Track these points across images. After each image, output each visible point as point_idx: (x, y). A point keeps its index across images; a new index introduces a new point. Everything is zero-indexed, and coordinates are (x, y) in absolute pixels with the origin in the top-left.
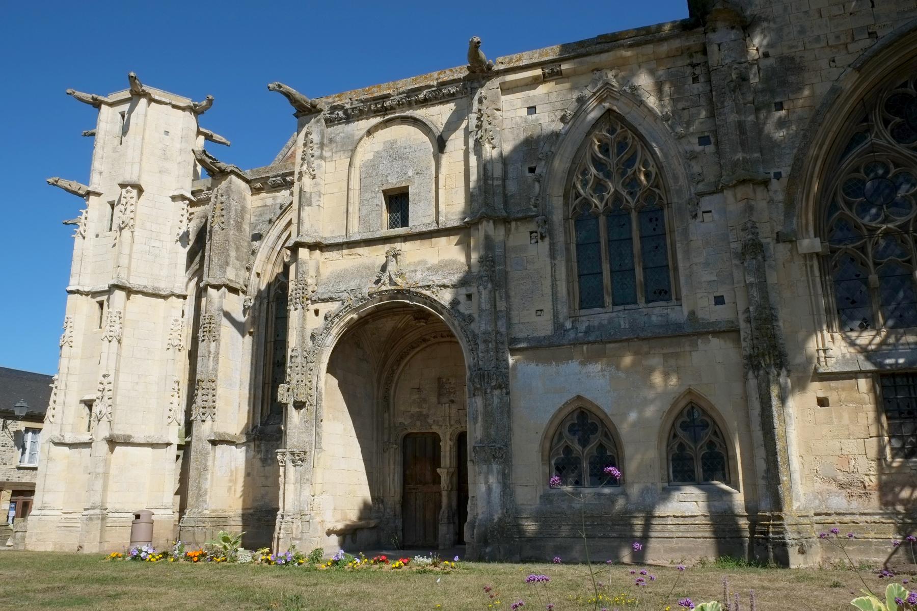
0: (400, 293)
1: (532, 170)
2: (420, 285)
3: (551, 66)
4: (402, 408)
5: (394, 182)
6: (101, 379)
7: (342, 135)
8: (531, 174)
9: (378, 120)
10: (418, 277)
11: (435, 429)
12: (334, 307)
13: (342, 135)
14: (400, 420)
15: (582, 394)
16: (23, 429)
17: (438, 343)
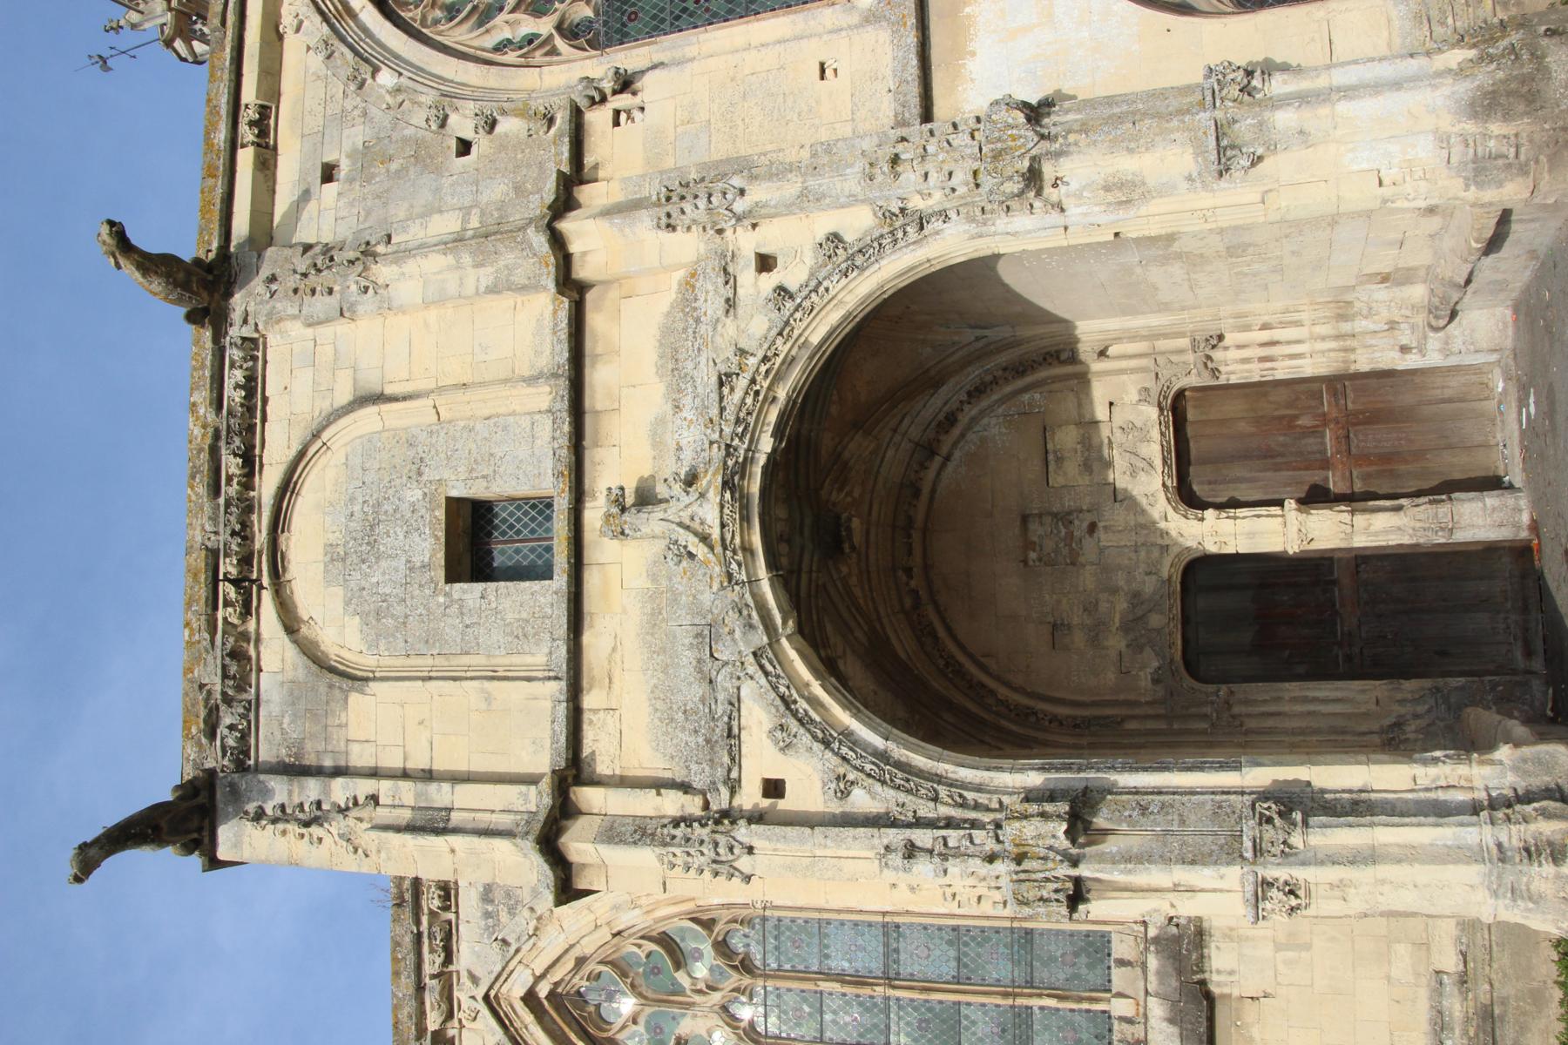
1: (464, 147)
4: (1111, 676)
6: (482, 145)
7: (286, 720)
8: (474, 149)
9: (267, 596)
13: (286, 720)
14: (1144, 680)
16: (835, 285)
17: (926, 567)
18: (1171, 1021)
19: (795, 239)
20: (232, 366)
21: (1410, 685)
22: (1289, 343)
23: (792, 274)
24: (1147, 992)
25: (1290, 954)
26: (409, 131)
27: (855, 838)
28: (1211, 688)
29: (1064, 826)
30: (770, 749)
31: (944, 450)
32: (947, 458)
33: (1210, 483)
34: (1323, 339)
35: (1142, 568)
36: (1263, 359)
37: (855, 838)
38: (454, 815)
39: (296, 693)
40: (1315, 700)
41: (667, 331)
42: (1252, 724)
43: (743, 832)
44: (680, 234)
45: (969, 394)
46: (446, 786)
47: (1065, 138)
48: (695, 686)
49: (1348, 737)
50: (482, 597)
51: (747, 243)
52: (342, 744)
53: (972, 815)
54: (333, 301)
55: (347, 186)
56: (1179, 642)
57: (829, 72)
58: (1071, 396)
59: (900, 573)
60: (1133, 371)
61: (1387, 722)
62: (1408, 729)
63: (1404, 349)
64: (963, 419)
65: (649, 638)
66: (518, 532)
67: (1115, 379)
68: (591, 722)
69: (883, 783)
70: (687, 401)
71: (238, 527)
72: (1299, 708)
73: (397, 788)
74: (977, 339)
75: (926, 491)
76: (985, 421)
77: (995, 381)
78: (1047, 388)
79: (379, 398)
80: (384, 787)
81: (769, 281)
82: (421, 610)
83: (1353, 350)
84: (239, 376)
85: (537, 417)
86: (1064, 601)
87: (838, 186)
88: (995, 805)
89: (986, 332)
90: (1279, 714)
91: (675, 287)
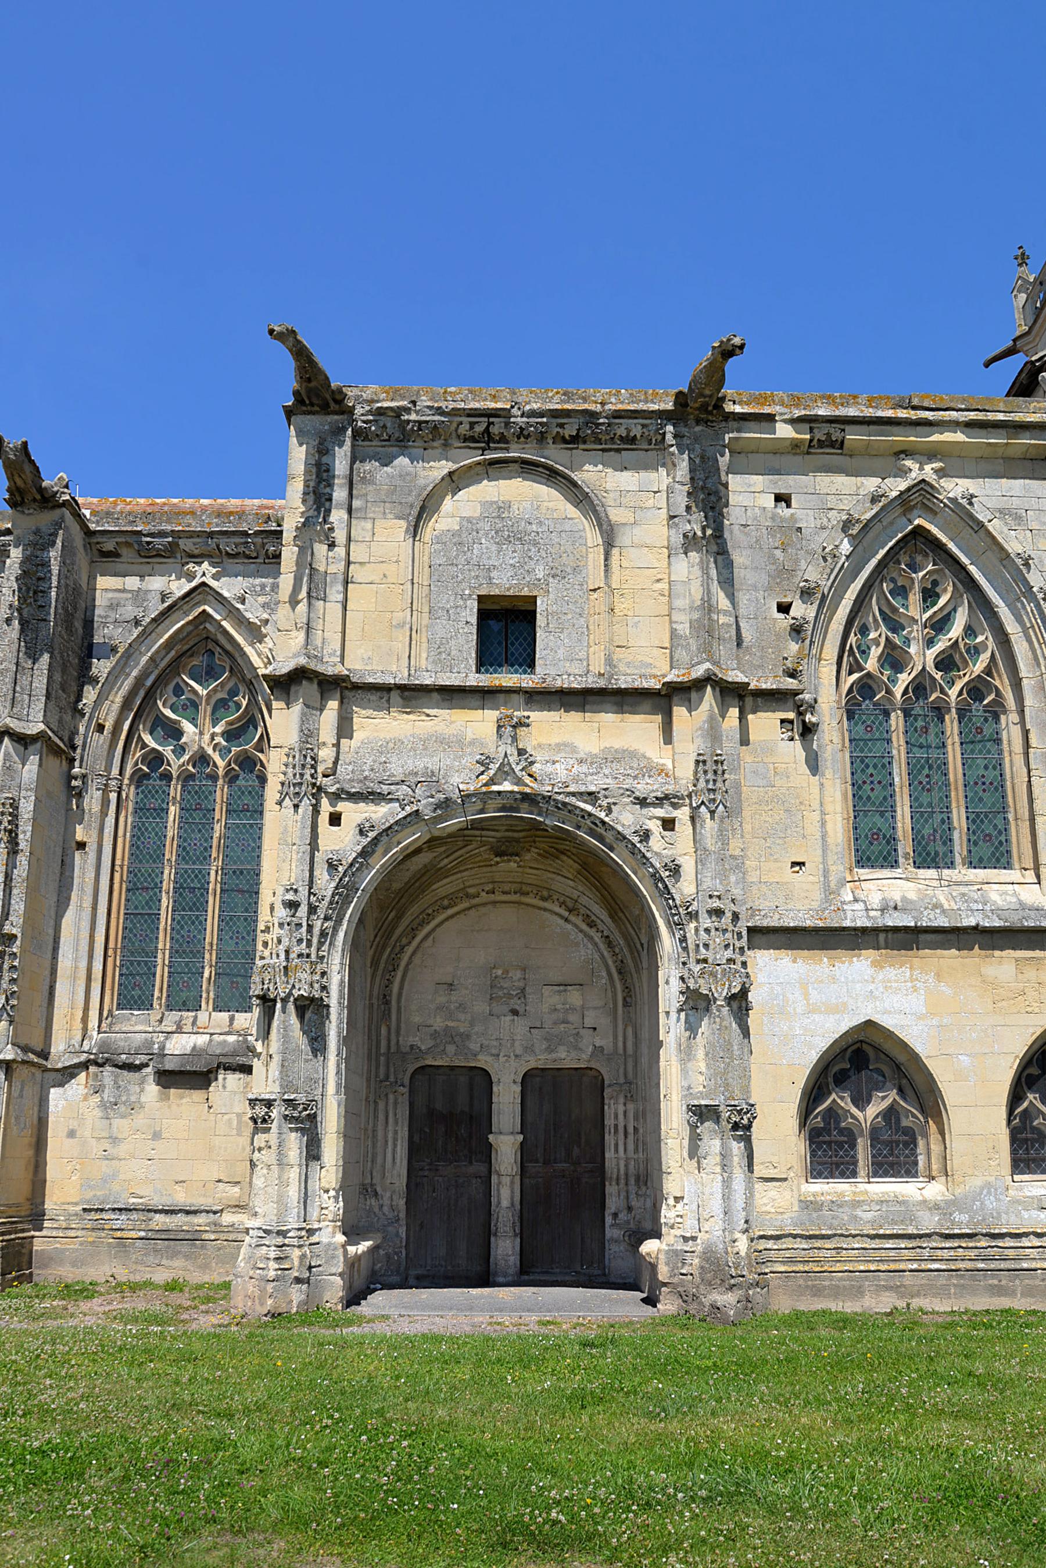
0: (529, 799)
1: (784, 608)
2: (571, 789)
3: (826, 428)
4: (417, 1019)
5: (504, 582)
6: (783, 622)
8: (782, 616)
10: (561, 772)
11: (483, 1061)
12: (381, 813)
15: (877, 1018)
17: (494, 903)
18: (194, 1048)
19: (677, 847)
20: (644, 426)
21: (402, 1202)
22: (625, 1144)
23: (656, 843)
24: (212, 1034)
25: (235, 1122)
26: (803, 564)
27: (303, 870)
28: (407, 1082)
29: (305, 994)
30: (359, 818)
31: (572, 918)
32: (566, 920)
33: (540, 1089)
34: (626, 1166)
35: (486, 1043)
36: (616, 1126)
37: (303, 870)
38: (322, 602)
39: (408, 478)
40: (395, 1146)
41: (633, 754)
42: (381, 1105)
43: (306, 804)
44: (692, 766)
45: (607, 937)
46: (340, 597)
47: (718, 1016)
48: (401, 770)
49: (369, 1164)
50: (467, 622)
51: (682, 815)
52: (371, 515)
53: (315, 941)
54: (682, 510)
55: (770, 515)
56: (436, 1063)
57: (797, 868)
58: (601, 1003)
59: (491, 886)
60: (615, 1044)
61: (379, 1189)
62: (373, 1201)
63: (615, 1215)
64: (592, 932)
65: (434, 738)
66: (513, 644)
67: (611, 1032)
68: (382, 698)
69: (336, 888)
70: (584, 768)
71: (525, 433)
72: (390, 1135)
73: (340, 561)
74: (642, 945)
75: (546, 905)
76: (590, 946)
77: (615, 954)
78: (609, 988)
79: (609, 545)
80: (340, 551)
81: (655, 826)
82: (461, 577)
83: (618, 1184)
84: (636, 431)
85: (585, 664)
86: (467, 992)
87: (709, 874)
88: (321, 953)
89: (645, 951)
90: (387, 1123)
91: (662, 761)
